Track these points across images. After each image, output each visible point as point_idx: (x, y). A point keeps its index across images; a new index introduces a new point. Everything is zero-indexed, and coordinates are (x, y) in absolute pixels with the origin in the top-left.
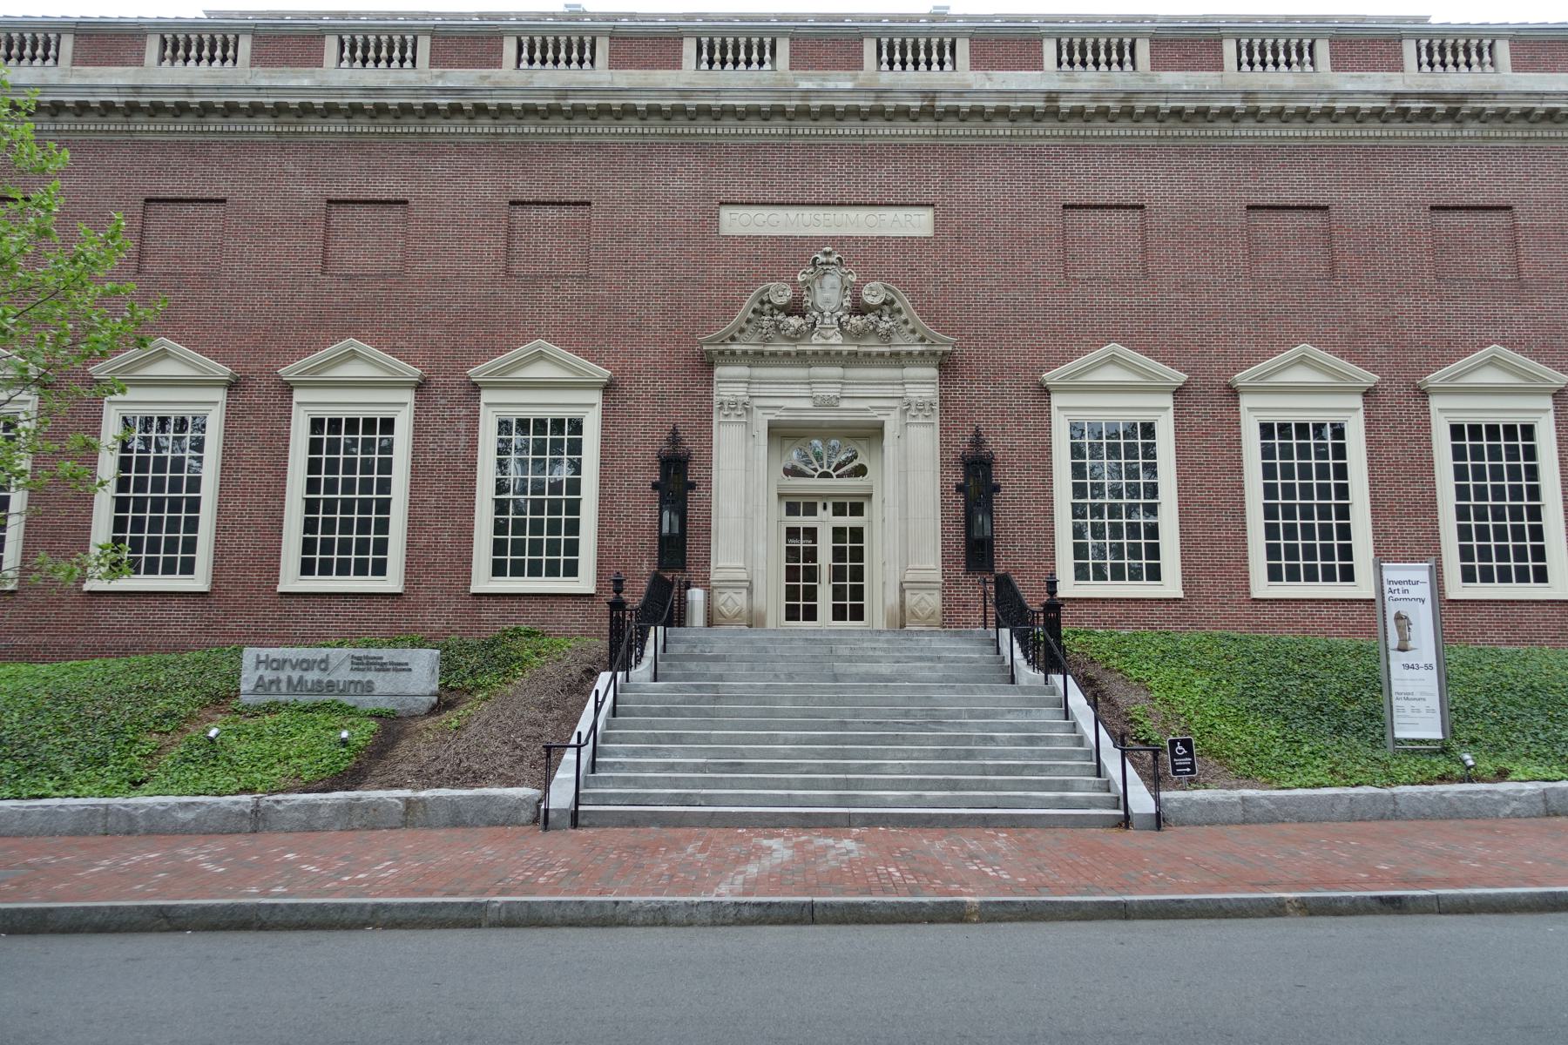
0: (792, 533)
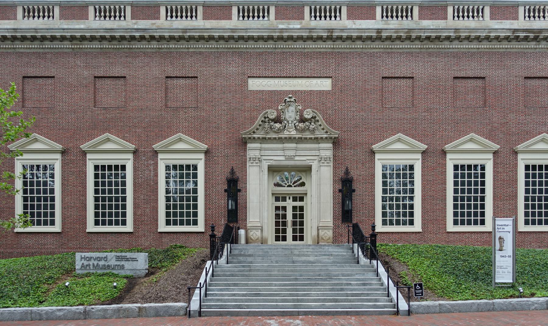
0: (277, 208)
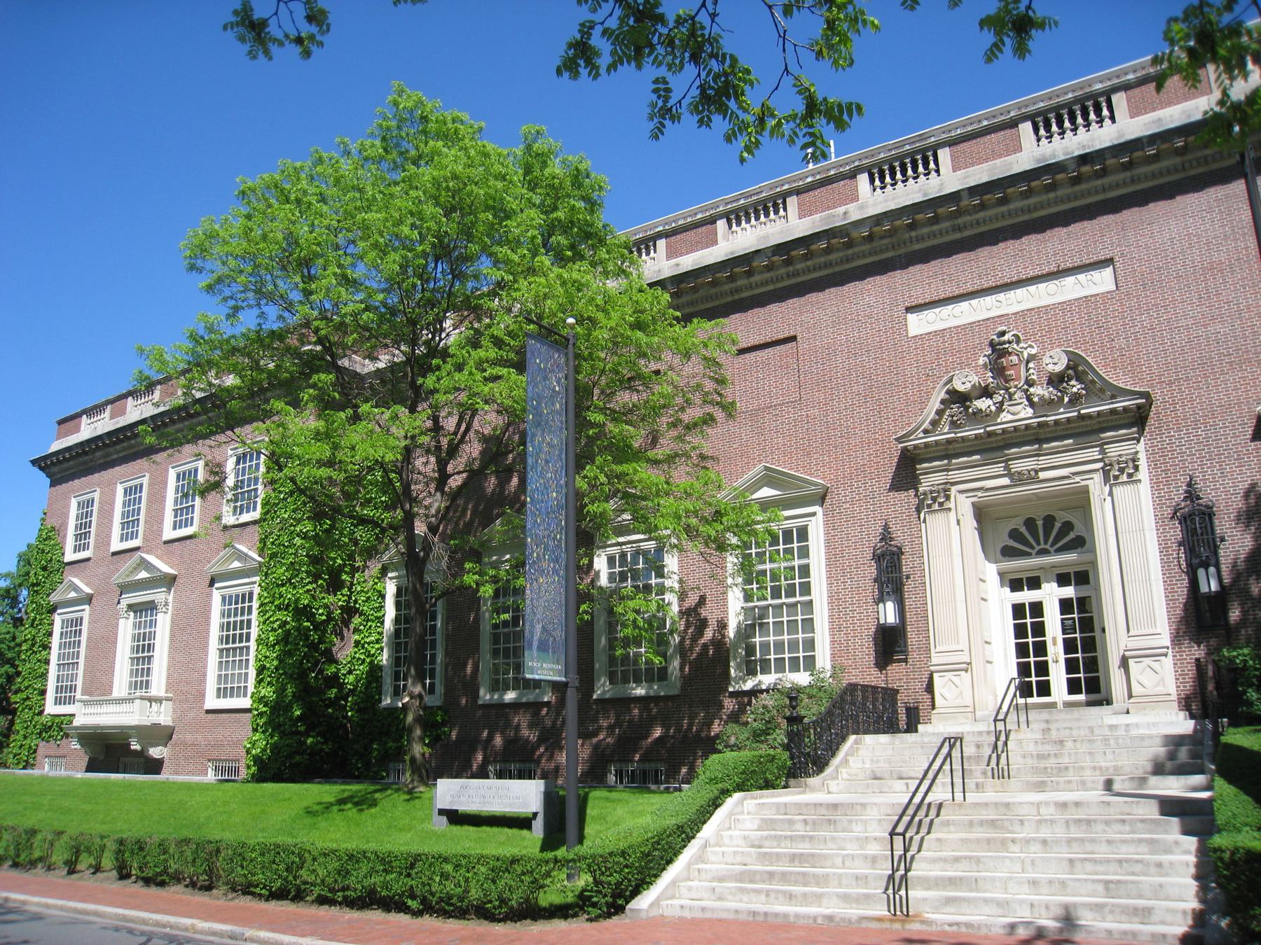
0: (1018, 610)
